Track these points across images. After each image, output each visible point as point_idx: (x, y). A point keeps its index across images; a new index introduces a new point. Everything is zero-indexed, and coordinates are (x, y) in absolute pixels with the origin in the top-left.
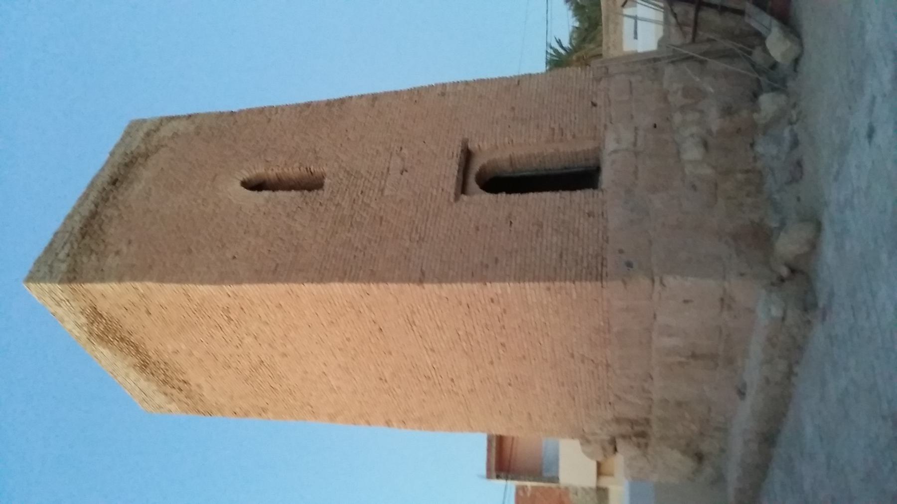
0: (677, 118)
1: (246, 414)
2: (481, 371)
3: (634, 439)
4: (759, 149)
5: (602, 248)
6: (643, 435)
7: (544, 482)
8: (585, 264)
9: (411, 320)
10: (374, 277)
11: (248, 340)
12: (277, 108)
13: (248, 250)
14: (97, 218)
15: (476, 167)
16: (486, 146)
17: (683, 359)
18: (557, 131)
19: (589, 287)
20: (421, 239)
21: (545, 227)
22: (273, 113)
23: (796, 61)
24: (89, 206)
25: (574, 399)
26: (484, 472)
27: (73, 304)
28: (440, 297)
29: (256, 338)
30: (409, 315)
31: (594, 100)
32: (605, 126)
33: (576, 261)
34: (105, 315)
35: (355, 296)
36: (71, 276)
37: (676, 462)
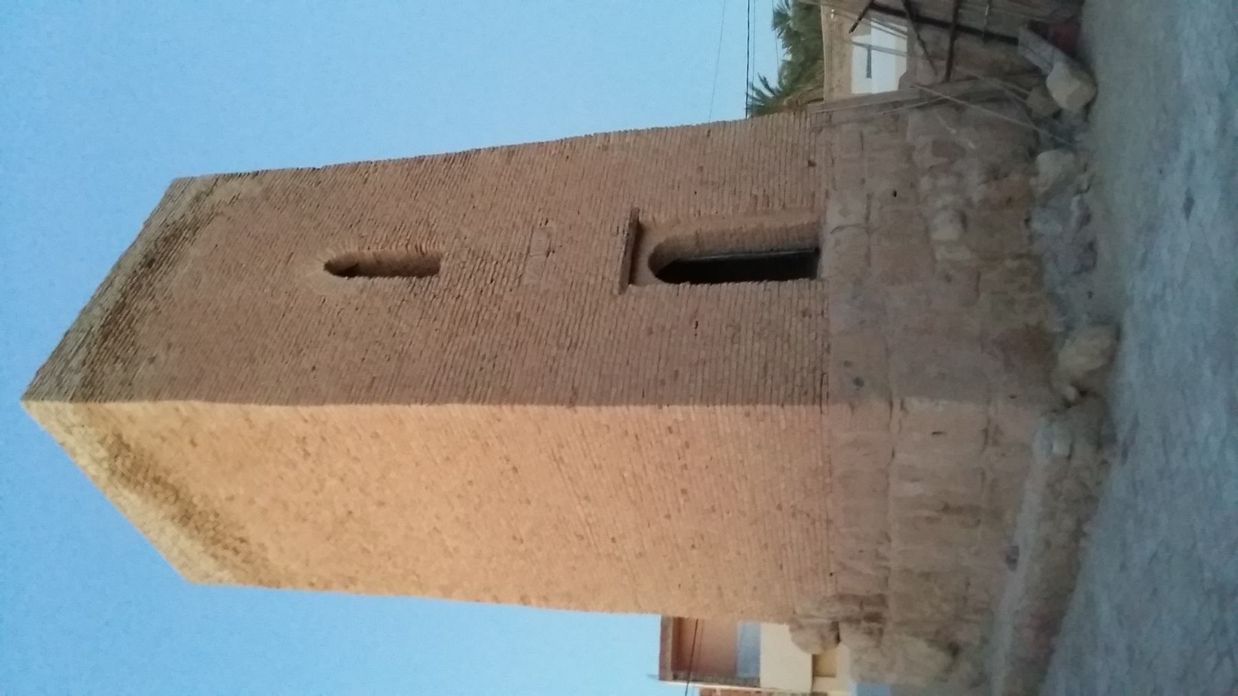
0: (925, 183)
1: (327, 586)
3: (864, 624)
4: (1036, 225)
6: (874, 618)
8: (798, 381)
10: (507, 396)
13: (333, 357)
15: (648, 248)
16: (662, 219)
19: (804, 412)
20: (573, 346)
23: (1088, 107)
24: (112, 298)
25: (781, 568)
26: (655, 669)
29: (342, 480)
30: (556, 449)
31: (812, 157)
32: (827, 194)
33: (786, 378)
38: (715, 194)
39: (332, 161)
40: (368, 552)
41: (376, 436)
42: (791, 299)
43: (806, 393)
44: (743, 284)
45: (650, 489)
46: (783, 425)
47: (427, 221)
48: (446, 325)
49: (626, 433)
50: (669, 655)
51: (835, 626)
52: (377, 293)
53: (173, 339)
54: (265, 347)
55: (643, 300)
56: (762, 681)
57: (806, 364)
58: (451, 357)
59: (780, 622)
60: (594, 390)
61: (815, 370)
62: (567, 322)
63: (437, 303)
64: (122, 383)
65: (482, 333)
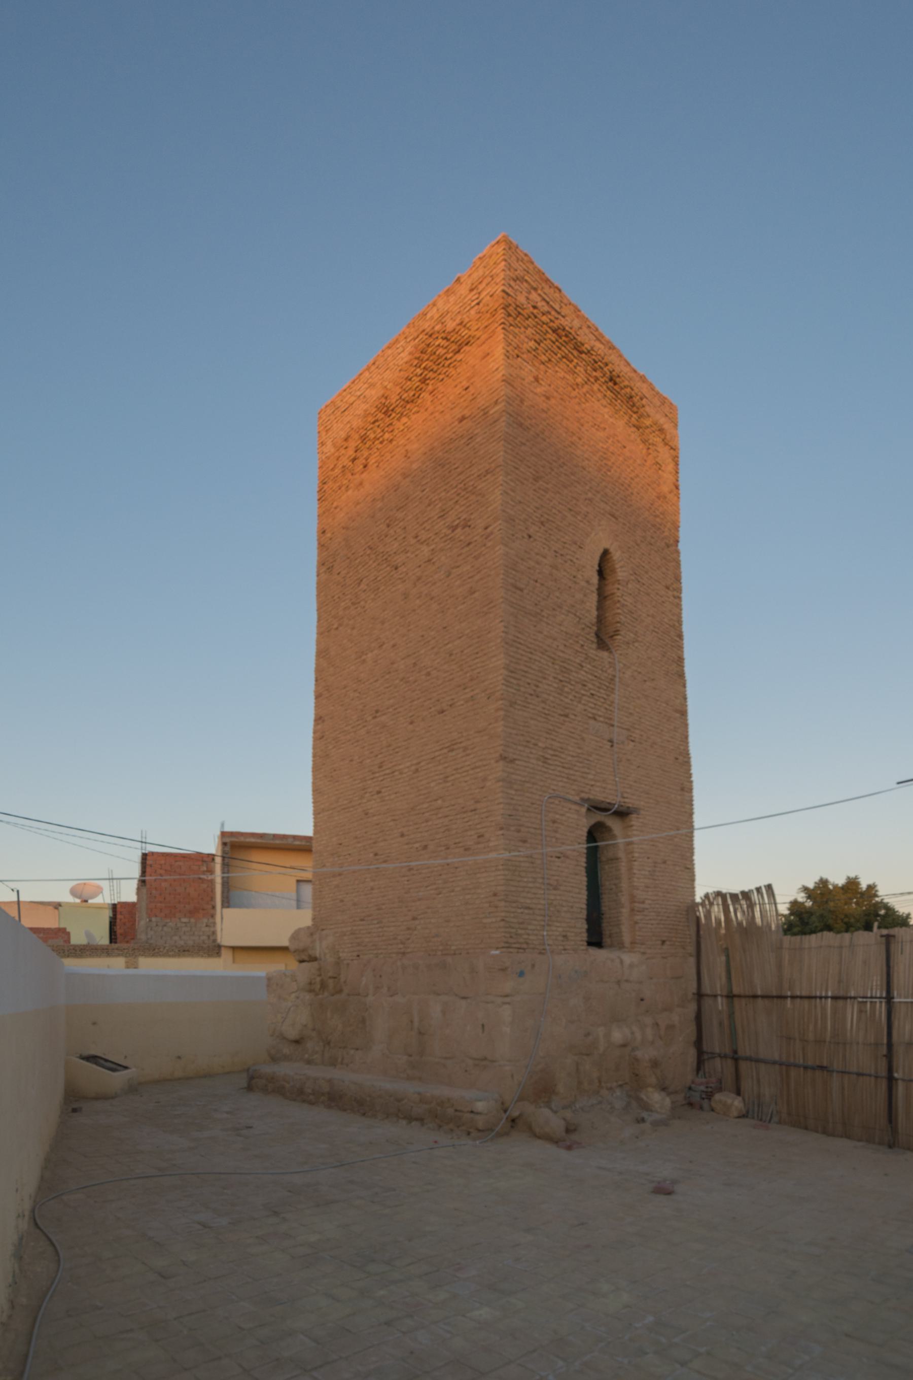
2: (392, 823)
3: (318, 979)
5: (534, 949)
7: (223, 892)
8: (520, 931)
9: (455, 747)
11: (425, 550)
12: (680, 598)
13: (537, 554)
14: (575, 353)
17: (416, 1024)
18: (642, 906)
20: (545, 760)
21: (555, 892)
22: (676, 593)
25: (362, 920)
26: (228, 828)
27: (473, 312)
28: (485, 779)
29: (429, 561)
30: (462, 745)
31: (668, 943)
32: (644, 953)
33: (522, 923)
34: (459, 357)
35: (486, 683)
36: (511, 309)
37: (297, 1018)
38: (647, 873)
39: (683, 558)
40: (359, 584)
41: (472, 592)
42: (575, 927)
43: (511, 937)
44: (586, 893)
45: (427, 821)
46: (485, 921)
47: (637, 641)
48: (561, 654)
49: (477, 802)
50: (242, 839)
51: (313, 959)
52: (585, 595)
53: (553, 401)
54: (546, 491)
55: (575, 816)
57: (531, 937)
58: (538, 658)
59: (314, 919)
60: (514, 777)
61: (527, 943)
62: (563, 756)
63: (577, 647)
64: (517, 347)
65: (555, 685)
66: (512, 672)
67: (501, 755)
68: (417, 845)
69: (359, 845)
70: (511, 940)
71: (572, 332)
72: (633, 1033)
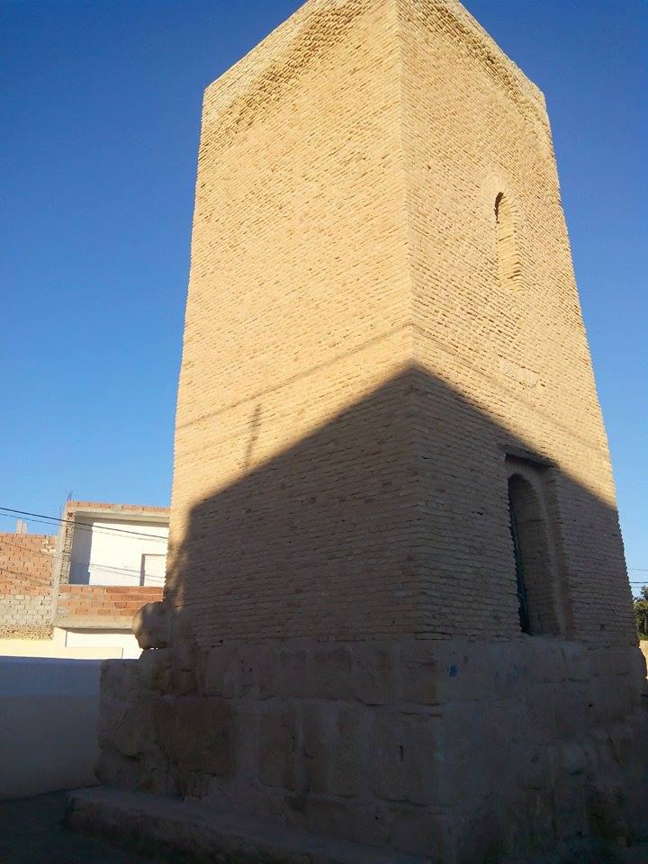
8: (444, 610)
18: (575, 579)
34: (349, 25)
35: (389, 309)
41: (369, 218)
43: (434, 617)
53: (442, 62)
56: (90, 581)
57: (458, 619)
60: (427, 413)
66: (419, 297)
67: (411, 387)
68: (304, 498)
69: (228, 501)
70: (434, 622)
71: (407, 105)
72: (586, 754)
